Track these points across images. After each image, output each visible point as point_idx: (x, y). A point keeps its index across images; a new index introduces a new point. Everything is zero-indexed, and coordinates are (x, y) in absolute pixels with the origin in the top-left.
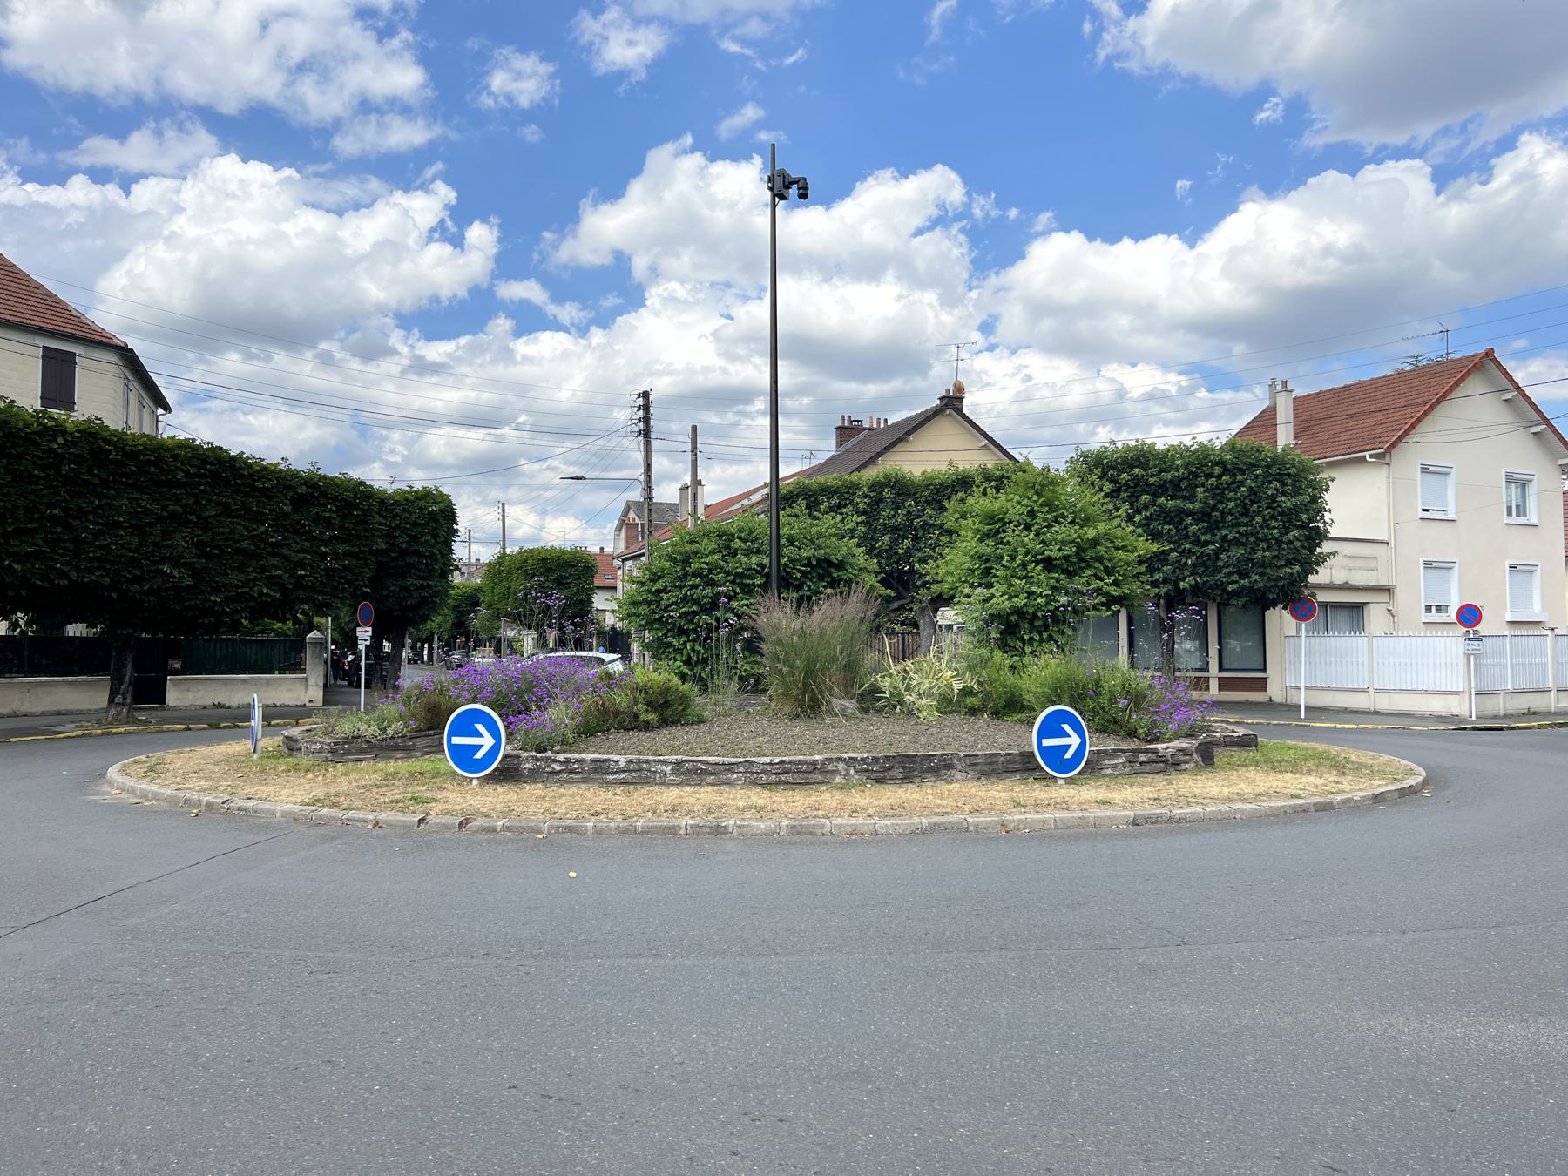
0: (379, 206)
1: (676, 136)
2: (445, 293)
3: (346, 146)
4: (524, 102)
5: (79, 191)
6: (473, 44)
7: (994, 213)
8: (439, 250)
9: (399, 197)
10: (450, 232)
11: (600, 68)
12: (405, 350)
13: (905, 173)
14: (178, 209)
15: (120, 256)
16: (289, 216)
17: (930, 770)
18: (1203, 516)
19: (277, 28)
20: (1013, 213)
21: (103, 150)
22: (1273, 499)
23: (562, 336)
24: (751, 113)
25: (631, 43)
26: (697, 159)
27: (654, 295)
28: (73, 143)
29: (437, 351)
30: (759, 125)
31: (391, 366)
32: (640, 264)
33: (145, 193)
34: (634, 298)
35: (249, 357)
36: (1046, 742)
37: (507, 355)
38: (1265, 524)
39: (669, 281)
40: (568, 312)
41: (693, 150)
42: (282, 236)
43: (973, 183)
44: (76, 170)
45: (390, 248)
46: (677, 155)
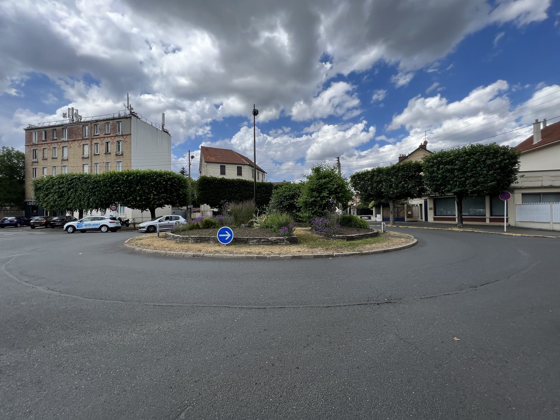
0: (352, 128)
1: (417, 95)
2: (365, 142)
3: (345, 118)
4: (380, 99)
5: (304, 138)
6: (369, 91)
7: (520, 88)
8: (364, 133)
9: (356, 125)
10: (366, 130)
11: (397, 87)
12: (357, 154)
13: (486, 85)
14: (318, 137)
15: (309, 147)
16: (336, 134)
17: (205, 240)
18: (460, 169)
19: (332, 100)
20: (527, 86)
21: (307, 130)
22: (484, 161)
23: (390, 146)
24: (436, 85)
25: (405, 79)
26: (423, 99)
27: (412, 132)
28: (302, 130)
29: (363, 153)
30: (438, 87)
31: (355, 157)
32: (407, 127)
33: (314, 135)
34: (407, 134)
35: (330, 160)
36: (220, 235)
37: (378, 152)
38: (481, 170)
39: (415, 128)
40: (391, 140)
41: (421, 97)
42: (335, 137)
43: (511, 82)
44: (303, 134)
45: (355, 135)
46: (416, 100)
